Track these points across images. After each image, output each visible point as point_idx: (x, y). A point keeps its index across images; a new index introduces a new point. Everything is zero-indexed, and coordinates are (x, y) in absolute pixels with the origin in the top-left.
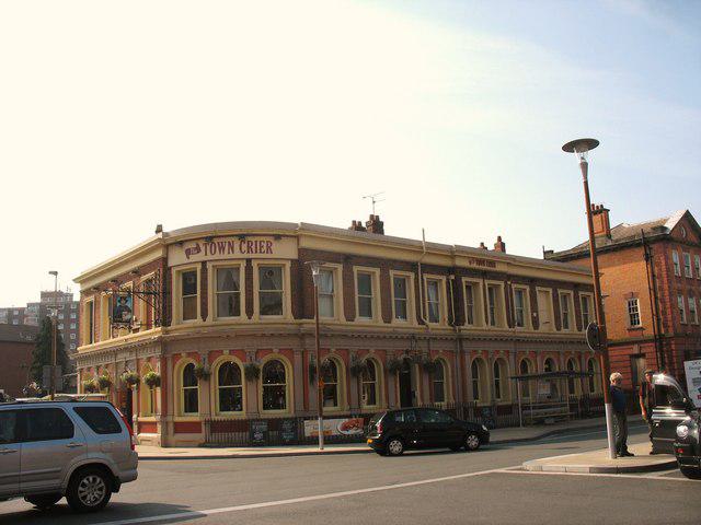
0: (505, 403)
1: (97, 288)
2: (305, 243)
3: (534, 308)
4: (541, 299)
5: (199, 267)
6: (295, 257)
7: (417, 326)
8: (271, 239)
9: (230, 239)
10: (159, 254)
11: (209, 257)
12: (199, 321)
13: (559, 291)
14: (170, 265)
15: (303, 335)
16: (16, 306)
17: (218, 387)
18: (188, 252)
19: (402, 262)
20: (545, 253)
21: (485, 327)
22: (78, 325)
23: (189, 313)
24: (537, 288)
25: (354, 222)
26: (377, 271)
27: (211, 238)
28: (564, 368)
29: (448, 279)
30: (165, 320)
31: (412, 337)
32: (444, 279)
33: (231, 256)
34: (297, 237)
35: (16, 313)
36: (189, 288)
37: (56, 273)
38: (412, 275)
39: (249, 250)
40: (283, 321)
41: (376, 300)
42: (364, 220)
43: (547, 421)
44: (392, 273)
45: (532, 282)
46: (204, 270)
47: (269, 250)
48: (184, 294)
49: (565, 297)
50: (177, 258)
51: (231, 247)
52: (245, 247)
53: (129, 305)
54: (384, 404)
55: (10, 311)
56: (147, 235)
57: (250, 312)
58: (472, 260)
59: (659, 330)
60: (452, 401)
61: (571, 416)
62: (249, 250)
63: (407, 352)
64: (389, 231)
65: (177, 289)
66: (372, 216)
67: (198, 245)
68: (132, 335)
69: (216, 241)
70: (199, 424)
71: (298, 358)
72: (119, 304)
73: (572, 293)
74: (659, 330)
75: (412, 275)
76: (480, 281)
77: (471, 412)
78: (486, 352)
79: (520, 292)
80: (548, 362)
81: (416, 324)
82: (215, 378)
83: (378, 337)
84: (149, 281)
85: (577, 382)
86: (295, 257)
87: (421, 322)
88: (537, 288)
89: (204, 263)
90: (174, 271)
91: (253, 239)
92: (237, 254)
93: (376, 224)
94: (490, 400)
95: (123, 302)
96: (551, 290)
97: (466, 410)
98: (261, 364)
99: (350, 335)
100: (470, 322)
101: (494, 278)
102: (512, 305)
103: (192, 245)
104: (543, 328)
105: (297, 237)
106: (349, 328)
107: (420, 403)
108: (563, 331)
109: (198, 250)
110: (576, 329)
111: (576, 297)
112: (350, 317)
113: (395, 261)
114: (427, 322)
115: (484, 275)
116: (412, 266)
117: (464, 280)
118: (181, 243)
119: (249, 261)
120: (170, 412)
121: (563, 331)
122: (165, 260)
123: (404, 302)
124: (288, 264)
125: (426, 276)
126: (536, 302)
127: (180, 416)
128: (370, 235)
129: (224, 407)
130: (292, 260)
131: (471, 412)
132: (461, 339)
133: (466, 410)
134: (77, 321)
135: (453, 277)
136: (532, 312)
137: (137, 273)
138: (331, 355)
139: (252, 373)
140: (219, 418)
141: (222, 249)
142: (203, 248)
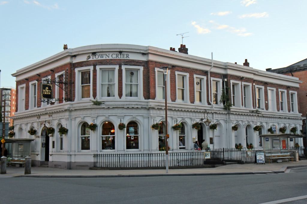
1: (27, 80)
3: (266, 99)
4: (269, 92)
13: (280, 90)
15: (150, 108)
17: (80, 136)
19: (200, 70)
24: (268, 88)
26: (188, 75)
29: (223, 82)
32: (221, 80)
43: (279, 161)
45: (266, 84)
48: (82, 84)
49: (282, 93)
52: (122, 57)
57: (120, 95)
59: (174, 118)
66: (182, 45)
68: (49, 105)
74: (174, 118)
75: (205, 78)
76: (239, 82)
79: (259, 89)
82: (100, 129)
84: (62, 75)
87: (209, 104)
88: (268, 88)
93: (183, 49)
98: (126, 122)
100: (234, 105)
102: (255, 96)
104: (270, 110)
108: (291, 112)
110: (287, 111)
111: (288, 93)
113: (197, 70)
114: (212, 103)
116: (205, 73)
121: (281, 111)
125: (212, 79)
127: (78, 152)
128: (178, 53)
135: (226, 80)
136: (265, 101)
137: (53, 71)
139: (121, 127)
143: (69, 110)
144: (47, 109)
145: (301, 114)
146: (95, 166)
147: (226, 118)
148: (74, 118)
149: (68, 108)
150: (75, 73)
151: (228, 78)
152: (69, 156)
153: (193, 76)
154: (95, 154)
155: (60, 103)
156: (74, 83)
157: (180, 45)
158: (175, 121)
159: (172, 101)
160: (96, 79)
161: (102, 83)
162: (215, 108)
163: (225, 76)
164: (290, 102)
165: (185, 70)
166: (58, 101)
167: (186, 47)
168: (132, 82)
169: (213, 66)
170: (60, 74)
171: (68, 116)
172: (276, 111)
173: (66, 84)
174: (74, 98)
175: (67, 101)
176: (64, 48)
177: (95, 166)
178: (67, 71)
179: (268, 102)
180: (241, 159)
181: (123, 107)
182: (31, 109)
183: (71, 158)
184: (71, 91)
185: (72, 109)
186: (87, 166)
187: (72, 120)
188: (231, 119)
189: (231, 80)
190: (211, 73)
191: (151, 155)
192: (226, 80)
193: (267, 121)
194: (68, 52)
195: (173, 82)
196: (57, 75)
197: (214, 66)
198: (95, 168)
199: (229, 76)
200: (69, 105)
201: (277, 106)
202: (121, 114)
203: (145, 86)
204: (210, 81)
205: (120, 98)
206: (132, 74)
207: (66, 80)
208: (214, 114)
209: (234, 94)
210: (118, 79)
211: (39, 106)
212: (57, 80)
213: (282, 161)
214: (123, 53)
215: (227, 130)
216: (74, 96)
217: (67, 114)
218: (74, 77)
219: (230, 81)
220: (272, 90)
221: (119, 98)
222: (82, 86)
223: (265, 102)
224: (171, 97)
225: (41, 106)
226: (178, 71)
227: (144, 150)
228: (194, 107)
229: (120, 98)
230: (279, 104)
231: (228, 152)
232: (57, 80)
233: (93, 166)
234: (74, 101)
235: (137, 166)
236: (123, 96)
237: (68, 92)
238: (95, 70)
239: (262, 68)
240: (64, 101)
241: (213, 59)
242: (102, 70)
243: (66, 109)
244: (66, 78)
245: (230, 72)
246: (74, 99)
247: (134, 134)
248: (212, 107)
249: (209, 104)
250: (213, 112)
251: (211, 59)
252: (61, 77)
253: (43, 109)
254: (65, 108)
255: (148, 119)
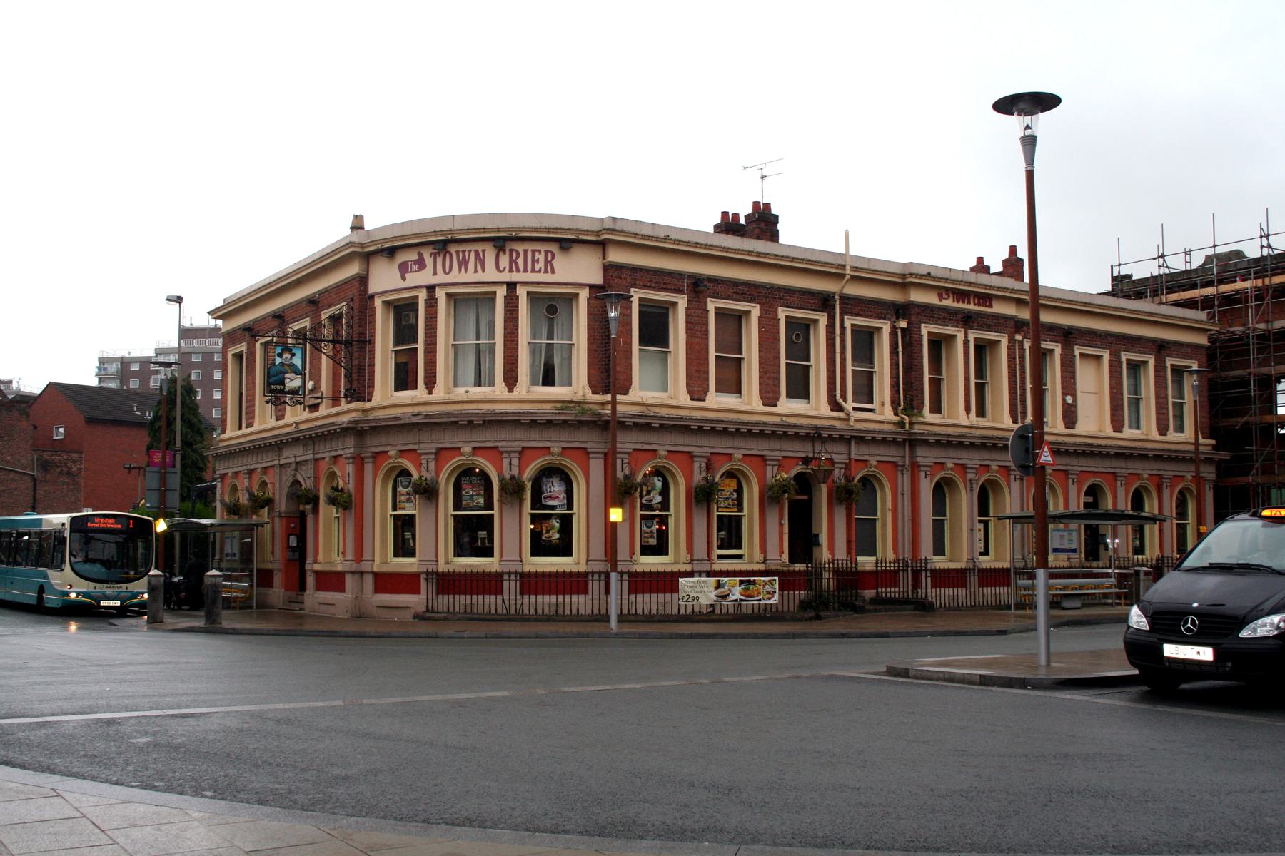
0: (953, 566)
1: (250, 331)
2: (615, 256)
3: (1069, 386)
5: (423, 295)
6: (597, 279)
7: (689, 403)
8: (554, 248)
9: (479, 247)
10: (353, 269)
11: (441, 278)
12: (420, 393)
13: (1124, 357)
14: (371, 290)
16: (135, 354)
17: (451, 512)
18: (404, 269)
20: (1114, 279)
21: (963, 419)
22: (224, 392)
23: (404, 379)
25: (725, 214)
27: (445, 243)
28: (1124, 505)
30: (359, 387)
31: (816, 435)
32: (886, 328)
33: (480, 277)
34: (602, 245)
35: (135, 367)
36: (404, 333)
37: (179, 300)
38: (823, 320)
39: (513, 265)
40: (1143, 437)
41: (881, 374)
42: (743, 210)
44: (782, 313)
46: (432, 302)
47: (549, 265)
48: (397, 343)
50: (385, 279)
51: (481, 260)
52: (504, 260)
53: (297, 361)
54: (684, 556)
55: (125, 362)
56: (336, 232)
58: (943, 292)
60: (890, 555)
61: (1118, 596)
62: (513, 265)
63: (806, 461)
64: (792, 234)
65: (385, 334)
66: (756, 204)
67: (420, 254)
69: (453, 249)
70: (417, 576)
71: (597, 466)
72: (278, 361)
73: (1152, 362)
77: (926, 580)
78: (963, 468)
79: (1178, 371)
80: (1093, 491)
81: (825, 410)
83: (949, 443)
85: (1151, 531)
86: (597, 279)
87: (836, 406)
88: (1078, 351)
89: (431, 289)
90: (378, 302)
91: (520, 247)
92: (490, 274)
94: (965, 556)
95: (287, 355)
96: (1106, 356)
97: (916, 574)
99: (694, 426)
101: (988, 328)
103: (411, 256)
105: (602, 245)
106: (695, 414)
107: (826, 555)
109: (421, 264)
111: (1160, 369)
112: (697, 390)
113: (790, 291)
114: (849, 405)
115: (967, 320)
116: (824, 302)
117: (925, 329)
118: (391, 252)
119: (511, 286)
120: (367, 556)
122: (363, 280)
123: (870, 375)
124: (584, 295)
126: (1073, 377)
129: (540, 548)
130: (592, 287)
131: (926, 580)
132: (913, 442)
133: (916, 574)
134: (222, 385)
135: (903, 324)
136: (1064, 394)
137: (314, 303)
138: (871, 470)
140: (451, 568)
141: (463, 263)
142: (429, 261)
143: (353, 428)
144: (302, 427)
145: (1213, 442)
146: (430, 609)
147: (902, 454)
148: (370, 454)
149: (350, 422)
150: (373, 310)
151: (913, 318)
152: (357, 576)
153: (776, 312)
154: (430, 570)
155: (333, 406)
156: (371, 342)
157: (720, 215)
158: (704, 465)
159: (692, 399)
160: (435, 329)
161: (456, 343)
162: (856, 420)
163: (900, 310)
164: (1166, 397)
165: (742, 294)
166: (330, 402)
167: (774, 212)
168: (553, 339)
169: (848, 277)
170: (332, 310)
171: (352, 450)
172: (1109, 431)
173: (348, 343)
174: (371, 389)
175: (351, 402)
176: (352, 228)
177: (430, 609)
178: (351, 303)
179: (1075, 400)
180: (926, 594)
181: (456, 422)
182: (260, 424)
183: (362, 580)
184: (361, 368)
185: (362, 427)
186: (407, 608)
187: (366, 460)
188: (919, 459)
189: (923, 325)
190: (845, 299)
191: (592, 577)
192: (903, 324)
193: (1068, 468)
194: (350, 242)
195: (699, 334)
196: (325, 315)
197: (853, 277)
198: (428, 614)
199: (917, 310)
200: (354, 414)
201: (1113, 415)
202: (513, 444)
203: (595, 351)
204: (843, 328)
205: (511, 390)
206: (552, 310)
207: (348, 333)
208: (853, 443)
209: (940, 373)
210: (505, 329)
211: (280, 413)
212: (326, 332)
213: (674, 589)
214: (509, 246)
215: (905, 496)
216: (372, 386)
217: (350, 442)
218: (373, 322)
219: (920, 328)
220: (1098, 358)
221: (426, 391)
222: (396, 351)
223: (1064, 400)
224: (688, 385)
225: (286, 417)
226: (717, 296)
227: (588, 561)
228: (777, 419)
229: (511, 390)
230: (1122, 405)
231: (905, 573)
232: (325, 331)
233: (425, 609)
234: (370, 400)
235: (557, 611)
236: (632, 386)
237: (355, 370)
238: (432, 299)
239: (1095, 283)
240: (343, 400)
241: (851, 253)
242: (455, 300)
243: (345, 425)
244: (350, 327)
245: (917, 297)
246: (371, 394)
247: (736, 510)
248: (848, 420)
249: (839, 408)
250: (847, 435)
251: (843, 251)
252: (335, 319)
253: (291, 425)
254: (344, 423)
255: (602, 461)
